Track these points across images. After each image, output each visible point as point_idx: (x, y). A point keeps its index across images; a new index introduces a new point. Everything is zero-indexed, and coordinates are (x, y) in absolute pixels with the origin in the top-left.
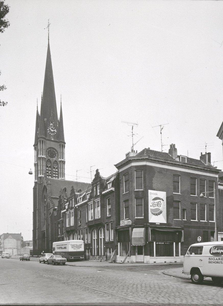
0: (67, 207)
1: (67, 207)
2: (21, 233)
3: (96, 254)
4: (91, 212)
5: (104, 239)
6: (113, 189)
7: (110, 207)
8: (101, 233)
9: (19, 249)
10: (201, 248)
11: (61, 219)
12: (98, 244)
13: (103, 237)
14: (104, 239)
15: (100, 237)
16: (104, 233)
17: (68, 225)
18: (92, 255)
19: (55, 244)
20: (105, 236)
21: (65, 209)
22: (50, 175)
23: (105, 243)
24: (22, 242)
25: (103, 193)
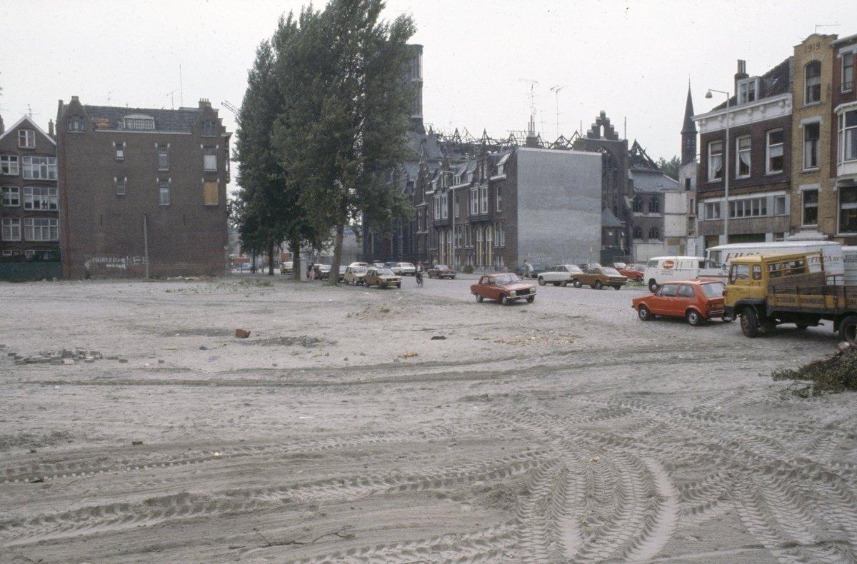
0: (434, 187)
1: (434, 187)
2: (249, 332)
3: (481, 264)
4: (474, 202)
5: (493, 243)
6: (504, 176)
7: (500, 199)
8: (488, 234)
9: (351, 480)
10: (657, 262)
11: (424, 203)
12: (484, 249)
13: (490, 240)
14: (493, 243)
15: (487, 240)
16: (493, 234)
17: (476, 211)
18: (475, 264)
19: (615, 264)
20: (493, 238)
21: (430, 188)
22: (277, 271)
23: (494, 249)
24: (684, 246)
25: (492, 178)
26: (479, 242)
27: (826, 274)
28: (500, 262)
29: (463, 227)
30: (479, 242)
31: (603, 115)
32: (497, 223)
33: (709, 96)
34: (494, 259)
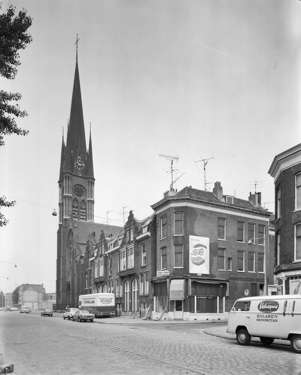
0: (95, 255)
1: (95, 255)
3: (128, 310)
4: (123, 260)
5: (138, 292)
6: (149, 234)
8: (134, 285)
10: (248, 303)
14: (138, 292)
15: (126, 291)
16: (138, 285)
17: (97, 276)
18: (123, 310)
20: (138, 288)
23: (140, 297)
25: (138, 238)
26: (134, 292)
27: (285, 313)
28: (120, 308)
29: (114, 282)
30: (134, 292)
31: (150, 206)
32: (142, 275)
33: (16, 285)
34: (139, 306)
